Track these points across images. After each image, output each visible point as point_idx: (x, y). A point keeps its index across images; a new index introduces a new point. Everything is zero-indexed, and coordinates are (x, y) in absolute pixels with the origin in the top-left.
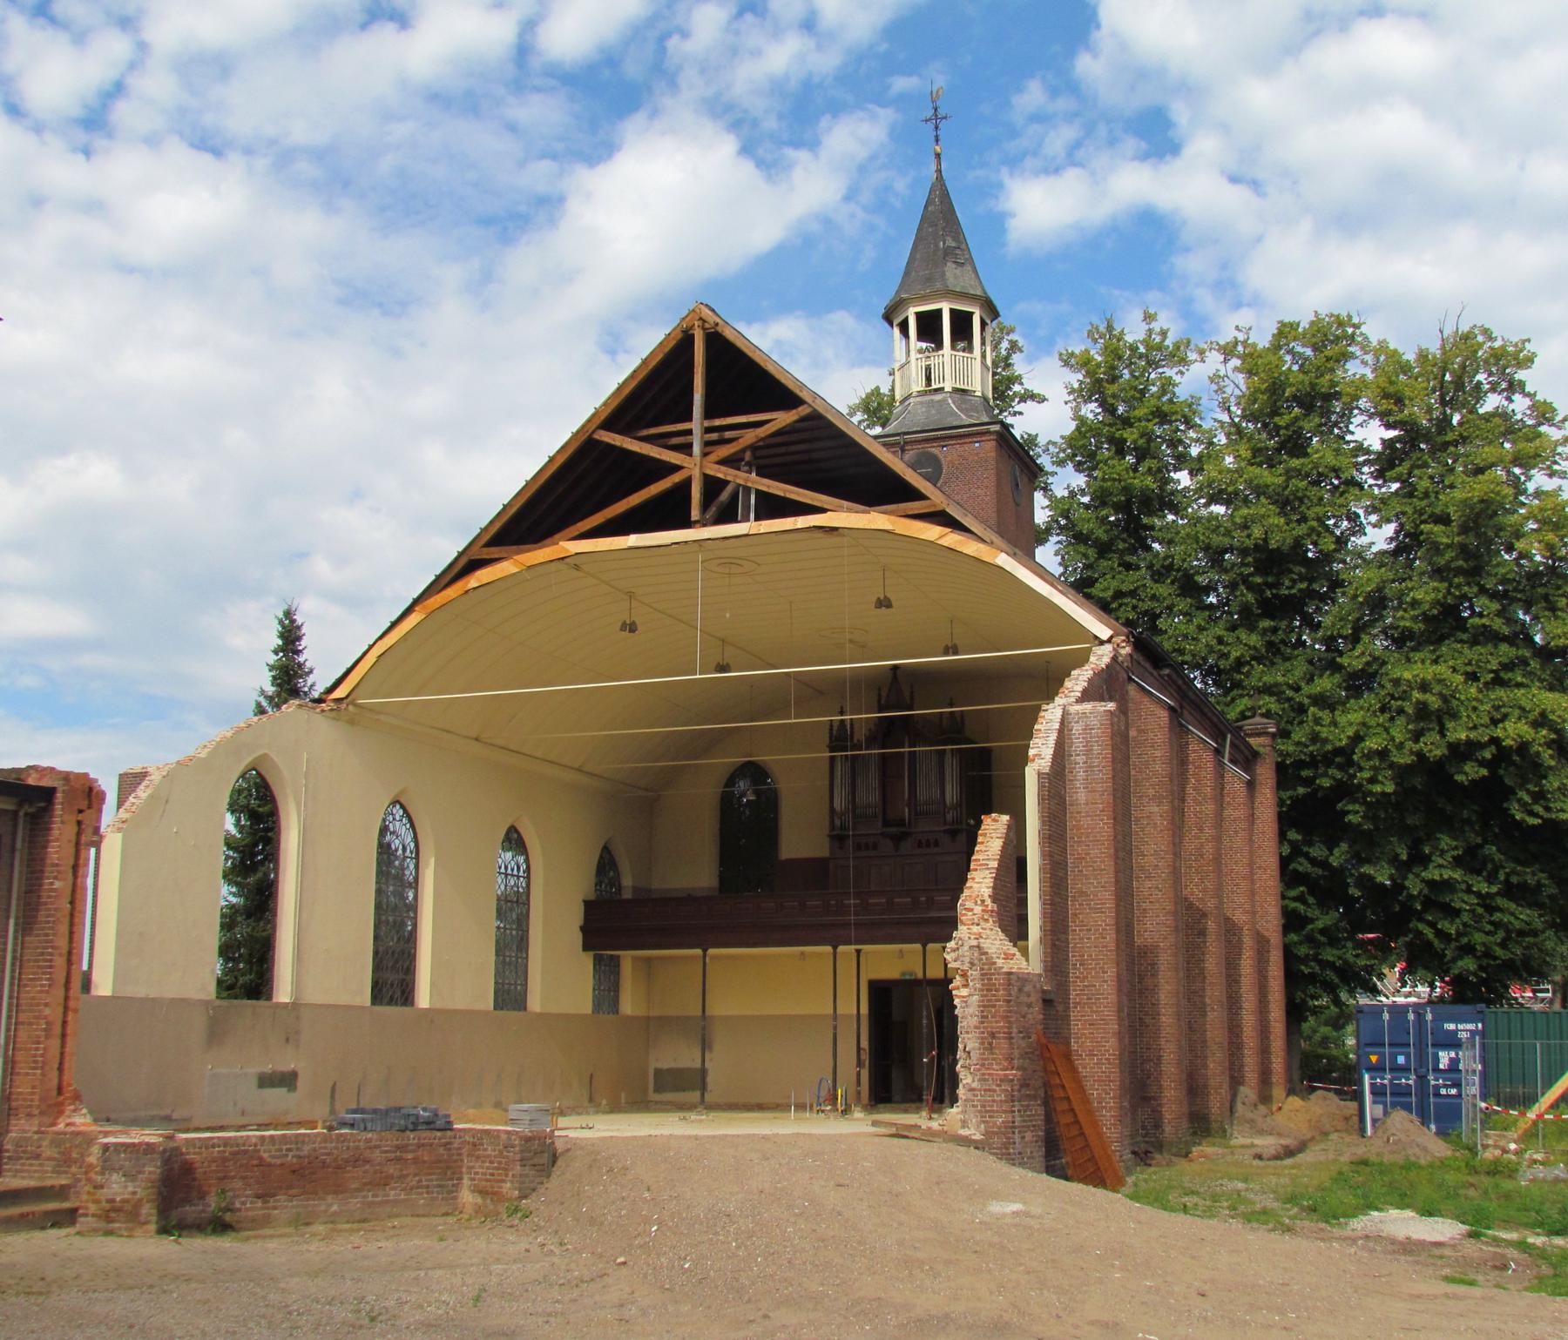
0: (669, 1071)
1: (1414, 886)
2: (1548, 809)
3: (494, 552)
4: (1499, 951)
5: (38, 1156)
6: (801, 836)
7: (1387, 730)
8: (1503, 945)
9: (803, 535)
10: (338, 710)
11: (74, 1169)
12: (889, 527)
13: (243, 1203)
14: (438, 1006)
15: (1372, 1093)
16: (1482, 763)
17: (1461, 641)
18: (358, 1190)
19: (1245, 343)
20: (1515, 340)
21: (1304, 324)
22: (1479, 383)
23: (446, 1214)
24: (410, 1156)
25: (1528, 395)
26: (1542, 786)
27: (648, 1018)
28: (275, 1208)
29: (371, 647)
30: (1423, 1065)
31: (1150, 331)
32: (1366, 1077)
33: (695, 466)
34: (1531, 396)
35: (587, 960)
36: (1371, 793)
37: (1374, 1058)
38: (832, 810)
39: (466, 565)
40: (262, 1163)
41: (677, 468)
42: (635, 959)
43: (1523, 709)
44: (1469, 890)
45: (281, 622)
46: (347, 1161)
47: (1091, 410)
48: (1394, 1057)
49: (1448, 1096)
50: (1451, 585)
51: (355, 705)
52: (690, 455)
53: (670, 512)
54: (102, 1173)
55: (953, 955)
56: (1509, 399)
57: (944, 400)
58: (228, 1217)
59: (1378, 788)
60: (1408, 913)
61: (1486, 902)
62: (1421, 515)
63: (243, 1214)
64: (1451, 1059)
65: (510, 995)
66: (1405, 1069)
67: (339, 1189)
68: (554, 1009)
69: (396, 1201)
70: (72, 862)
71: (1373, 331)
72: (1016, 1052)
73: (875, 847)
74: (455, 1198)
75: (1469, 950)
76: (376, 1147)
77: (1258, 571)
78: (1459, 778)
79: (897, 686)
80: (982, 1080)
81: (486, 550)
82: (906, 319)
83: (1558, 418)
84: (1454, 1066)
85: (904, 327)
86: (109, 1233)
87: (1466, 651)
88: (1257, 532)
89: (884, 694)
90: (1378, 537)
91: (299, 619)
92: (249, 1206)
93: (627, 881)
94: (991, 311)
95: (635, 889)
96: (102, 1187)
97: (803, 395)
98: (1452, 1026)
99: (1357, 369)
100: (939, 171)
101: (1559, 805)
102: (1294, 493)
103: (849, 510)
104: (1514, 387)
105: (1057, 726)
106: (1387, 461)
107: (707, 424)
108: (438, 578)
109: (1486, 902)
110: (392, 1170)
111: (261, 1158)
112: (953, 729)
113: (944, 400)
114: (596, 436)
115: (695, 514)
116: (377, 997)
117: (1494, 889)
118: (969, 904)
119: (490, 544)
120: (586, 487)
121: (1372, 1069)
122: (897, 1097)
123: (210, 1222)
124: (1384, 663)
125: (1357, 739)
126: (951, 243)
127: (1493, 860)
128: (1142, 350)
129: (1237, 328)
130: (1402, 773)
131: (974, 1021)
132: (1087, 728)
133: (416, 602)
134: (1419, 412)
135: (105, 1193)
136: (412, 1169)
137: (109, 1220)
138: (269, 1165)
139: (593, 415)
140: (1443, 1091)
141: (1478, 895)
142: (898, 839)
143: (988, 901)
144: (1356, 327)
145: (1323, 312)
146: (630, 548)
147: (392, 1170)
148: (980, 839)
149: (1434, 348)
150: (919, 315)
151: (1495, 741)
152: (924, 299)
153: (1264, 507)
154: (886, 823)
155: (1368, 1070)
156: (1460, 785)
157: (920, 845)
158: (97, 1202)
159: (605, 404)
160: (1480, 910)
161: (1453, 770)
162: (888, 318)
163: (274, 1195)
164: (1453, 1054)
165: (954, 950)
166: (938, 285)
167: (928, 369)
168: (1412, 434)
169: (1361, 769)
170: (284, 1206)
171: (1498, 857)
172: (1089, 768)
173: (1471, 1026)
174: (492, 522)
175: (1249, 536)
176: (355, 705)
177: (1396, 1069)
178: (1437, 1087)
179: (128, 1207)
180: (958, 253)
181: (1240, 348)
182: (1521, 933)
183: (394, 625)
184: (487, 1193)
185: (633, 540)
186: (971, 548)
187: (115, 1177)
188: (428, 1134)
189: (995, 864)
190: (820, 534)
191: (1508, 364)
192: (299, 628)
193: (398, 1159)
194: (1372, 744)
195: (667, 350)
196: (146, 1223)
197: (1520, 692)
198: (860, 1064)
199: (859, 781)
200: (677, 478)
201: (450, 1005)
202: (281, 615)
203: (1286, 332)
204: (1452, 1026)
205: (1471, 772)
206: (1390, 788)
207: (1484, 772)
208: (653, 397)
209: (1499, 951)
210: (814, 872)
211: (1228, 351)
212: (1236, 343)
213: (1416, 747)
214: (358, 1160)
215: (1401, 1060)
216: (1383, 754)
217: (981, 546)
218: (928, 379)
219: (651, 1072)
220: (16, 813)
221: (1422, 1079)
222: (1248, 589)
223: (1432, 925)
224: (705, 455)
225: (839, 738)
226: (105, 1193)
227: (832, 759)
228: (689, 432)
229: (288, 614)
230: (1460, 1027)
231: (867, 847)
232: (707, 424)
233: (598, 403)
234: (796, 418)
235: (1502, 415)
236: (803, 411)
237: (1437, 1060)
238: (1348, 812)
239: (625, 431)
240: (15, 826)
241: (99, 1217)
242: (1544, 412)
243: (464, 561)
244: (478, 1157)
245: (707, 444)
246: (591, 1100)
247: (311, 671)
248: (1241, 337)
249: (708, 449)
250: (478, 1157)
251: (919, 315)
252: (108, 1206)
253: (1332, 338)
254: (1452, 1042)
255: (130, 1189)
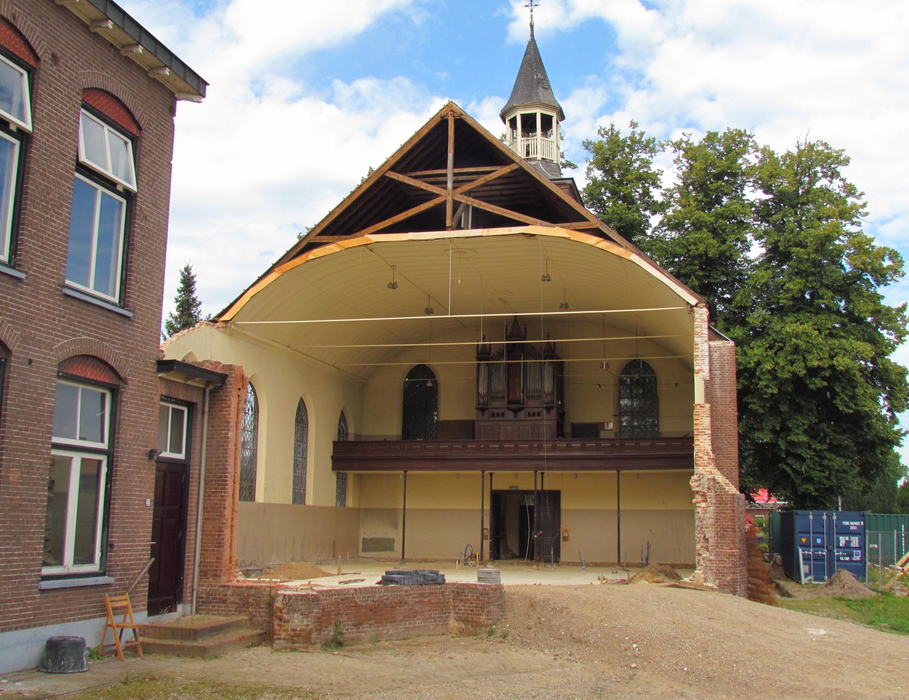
0: (372, 539)
1: (782, 445)
2: (856, 404)
3: (324, 239)
4: (825, 481)
5: (224, 601)
6: (452, 407)
7: (773, 359)
8: (828, 478)
9: (514, 238)
10: (226, 327)
11: (250, 609)
12: (566, 235)
13: (347, 630)
14: (267, 501)
15: (804, 559)
16: (824, 378)
17: (810, 312)
18: (402, 620)
19: (687, 143)
20: (837, 149)
21: (721, 134)
22: (816, 173)
23: (444, 634)
24: (426, 600)
25: (841, 180)
26: (854, 393)
27: (359, 509)
28: (362, 632)
29: (246, 292)
30: (831, 544)
31: (633, 133)
32: (800, 550)
33: (447, 194)
34: (843, 180)
35: (333, 477)
36: (766, 393)
37: (804, 540)
38: (478, 394)
39: (306, 246)
40: (356, 605)
41: (431, 196)
42: (355, 475)
43: (846, 350)
44: (810, 448)
45: (182, 273)
46: (396, 603)
47: (598, 174)
48: (815, 540)
49: (844, 561)
50: (807, 281)
51: (235, 325)
52: (446, 188)
53: (433, 220)
54: (289, 614)
55: (697, 483)
56: (831, 182)
57: (537, 164)
58: (340, 638)
59: (770, 391)
60: (777, 459)
61: (819, 454)
62: (789, 241)
63: (347, 635)
64: (846, 541)
65: (299, 495)
66: (821, 546)
67: (393, 620)
68: (319, 504)
69: (420, 627)
70: (235, 421)
71: (762, 138)
72: (737, 540)
73: (503, 415)
74: (447, 624)
75: (809, 480)
76: (410, 595)
77: (701, 269)
78: (812, 386)
79: (517, 327)
80: (717, 555)
81: (319, 237)
82: (515, 117)
83: (857, 194)
84: (848, 544)
85: (513, 123)
86: (293, 650)
87: (813, 317)
88: (702, 248)
89: (509, 328)
90: (756, 251)
91: (193, 273)
92: (349, 631)
93: (351, 430)
94: (562, 116)
95: (355, 435)
96: (288, 622)
97: (513, 158)
98: (847, 523)
99: (752, 159)
100: (532, 35)
101: (863, 403)
102: (719, 226)
103: (541, 225)
104: (834, 175)
105: (707, 354)
106: (764, 212)
107: (457, 171)
108: (288, 253)
109: (819, 454)
110: (417, 608)
111: (356, 602)
112: (550, 351)
113: (537, 164)
114: (387, 175)
115: (448, 223)
116: (294, 503)
117: (824, 447)
118: (700, 455)
119: (324, 233)
120: (379, 203)
121: (803, 546)
122: (502, 556)
123: (332, 641)
124: (770, 322)
125: (758, 364)
126: (540, 76)
127: (824, 432)
128: (629, 142)
129: (683, 134)
130: (781, 383)
131: (711, 521)
132: (721, 356)
133: (275, 266)
134: (785, 184)
135: (290, 625)
136: (427, 608)
137: (294, 642)
138: (360, 606)
139: (386, 163)
140: (842, 559)
141: (815, 450)
142: (516, 412)
143: (711, 453)
144: (750, 137)
145: (732, 128)
146: (409, 240)
147: (417, 608)
148: (695, 417)
149: (795, 151)
150: (523, 116)
151: (832, 367)
152: (526, 107)
153: (705, 234)
154: (509, 402)
155: (801, 546)
156: (811, 390)
157: (529, 415)
158: (286, 631)
159: (393, 156)
160: (816, 459)
161: (808, 382)
162: (503, 117)
163: (362, 624)
164: (847, 538)
165: (696, 481)
166: (535, 99)
167: (528, 146)
168: (781, 198)
169: (760, 379)
170: (368, 631)
171: (828, 431)
172: (723, 378)
173: (857, 523)
174: (322, 221)
175: (697, 249)
176: (235, 325)
177: (816, 546)
178: (838, 556)
179: (304, 634)
180: (543, 82)
181: (684, 145)
182: (838, 471)
183: (260, 279)
184: (468, 621)
185: (411, 236)
186: (615, 250)
187: (296, 615)
188: (433, 587)
189: (709, 432)
190: (522, 238)
191: (831, 161)
192: (193, 277)
193: (420, 602)
194: (768, 366)
195: (431, 127)
196: (315, 643)
197: (843, 341)
198: (483, 538)
199: (493, 378)
200: (437, 201)
201: (273, 501)
202: (183, 270)
203: (711, 137)
204: (847, 523)
205: (817, 383)
206: (775, 391)
207: (825, 384)
208: (425, 152)
209: (825, 481)
210: (467, 429)
211: (677, 146)
212: (682, 141)
213: (792, 369)
214: (402, 603)
215: (819, 541)
216: (773, 372)
217: (621, 249)
218: (528, 154)
219: (361, 541)
220: (204, 390)
221: (830, 552)
222: (696, 278)
223: (790, 466)
224: (454, 188)
225: (483, 354)
226: (290, 625)
227: (479, 365)
228: (445, 175)
229: (187, 269)
230: (852, 523)
231: (498, 415)
232: (457, 171)
233: (389, 155)
234: (509, 170)
235: (824, 191)
236: (514, 167)
237: (838, 541)
238: (750, 403)
239: (401, 172)
240: (204, 398)
241: (288, 640)
242: (850, 190)
243: (305, 243)
244: (461, 600)
245: (454, 182)
246: (334, 556)
247: (200, 303)
248: (685, 139)
249: (457, 185)
250: (461, 600)
251: (523, 116)
252: (292, 633)
253: (736, 143)
254: (847, 532)
255: (305, 623)
